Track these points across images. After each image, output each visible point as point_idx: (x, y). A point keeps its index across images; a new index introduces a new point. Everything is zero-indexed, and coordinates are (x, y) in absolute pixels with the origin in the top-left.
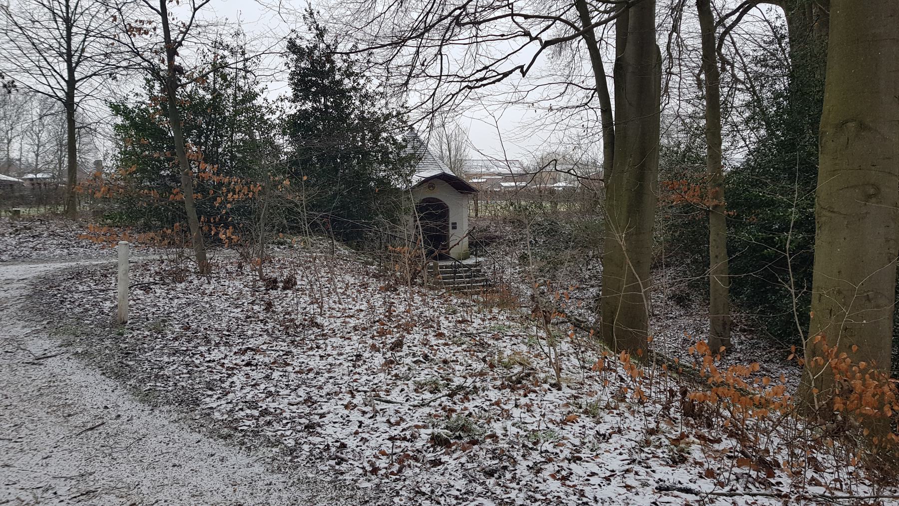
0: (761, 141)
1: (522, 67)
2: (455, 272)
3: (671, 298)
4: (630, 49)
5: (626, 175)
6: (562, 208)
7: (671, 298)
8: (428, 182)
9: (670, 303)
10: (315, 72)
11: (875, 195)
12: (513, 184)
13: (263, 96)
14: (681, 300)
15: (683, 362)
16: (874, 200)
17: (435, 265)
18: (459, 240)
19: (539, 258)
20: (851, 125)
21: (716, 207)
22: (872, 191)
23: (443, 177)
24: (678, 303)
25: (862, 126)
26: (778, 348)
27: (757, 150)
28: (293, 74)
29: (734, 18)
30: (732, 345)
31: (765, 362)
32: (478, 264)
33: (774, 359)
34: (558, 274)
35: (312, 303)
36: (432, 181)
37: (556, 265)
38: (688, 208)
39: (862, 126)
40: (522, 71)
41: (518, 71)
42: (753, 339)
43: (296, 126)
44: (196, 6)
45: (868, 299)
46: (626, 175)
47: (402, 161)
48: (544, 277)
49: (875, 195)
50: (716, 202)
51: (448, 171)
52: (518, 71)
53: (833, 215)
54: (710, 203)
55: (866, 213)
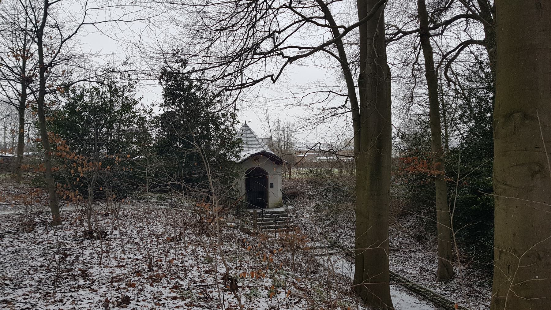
0: (471, 130)
1: (272, 76)
2: (262, 217)
3: (413, 237)
4: (369, 68)
5: (369, 153)
6: (345, 172)
7: (413, 237)
8: (254, 157)
9: (413, 240)
10: (177, 86)
11: (539, 172)
12: (325, 158)
13: (140, 102)
14: (420, 239)
15: (419, 284)
16: (539, 176)
17: (255, 211)
18: (275, 195)
19: (327, 208)
20: (517, 115)
21: (438, 175)
22: (537, 168)
23: (264, 153)
24: (418, 241)
25: (525, 116)
26: (487, 276)
27: (468, 137)
28: (165, 89)
29: (454, 53)
30: (454, 273)
31: (478, 286)
32: (287, 211)
33: (485, 284)
34: (339, 218)
35: (51, 263)
36: (256, 157)
37: (338, 212)
38: (421, 176)
39: (525, 116)
40: (272, 79)
41: (270, 78)
42: (469, 268)
43: (164, 120)
44: (65, 37)
45: (539, 258)
46: (369, 153)
47: (234, 144)
48: (330, 220)
49: (539, 172)
50: (438, 172)
51: (268, 150)
52: (270, 78)
53: (507, 187)
54: (436, 173)
55: (533, 186)
